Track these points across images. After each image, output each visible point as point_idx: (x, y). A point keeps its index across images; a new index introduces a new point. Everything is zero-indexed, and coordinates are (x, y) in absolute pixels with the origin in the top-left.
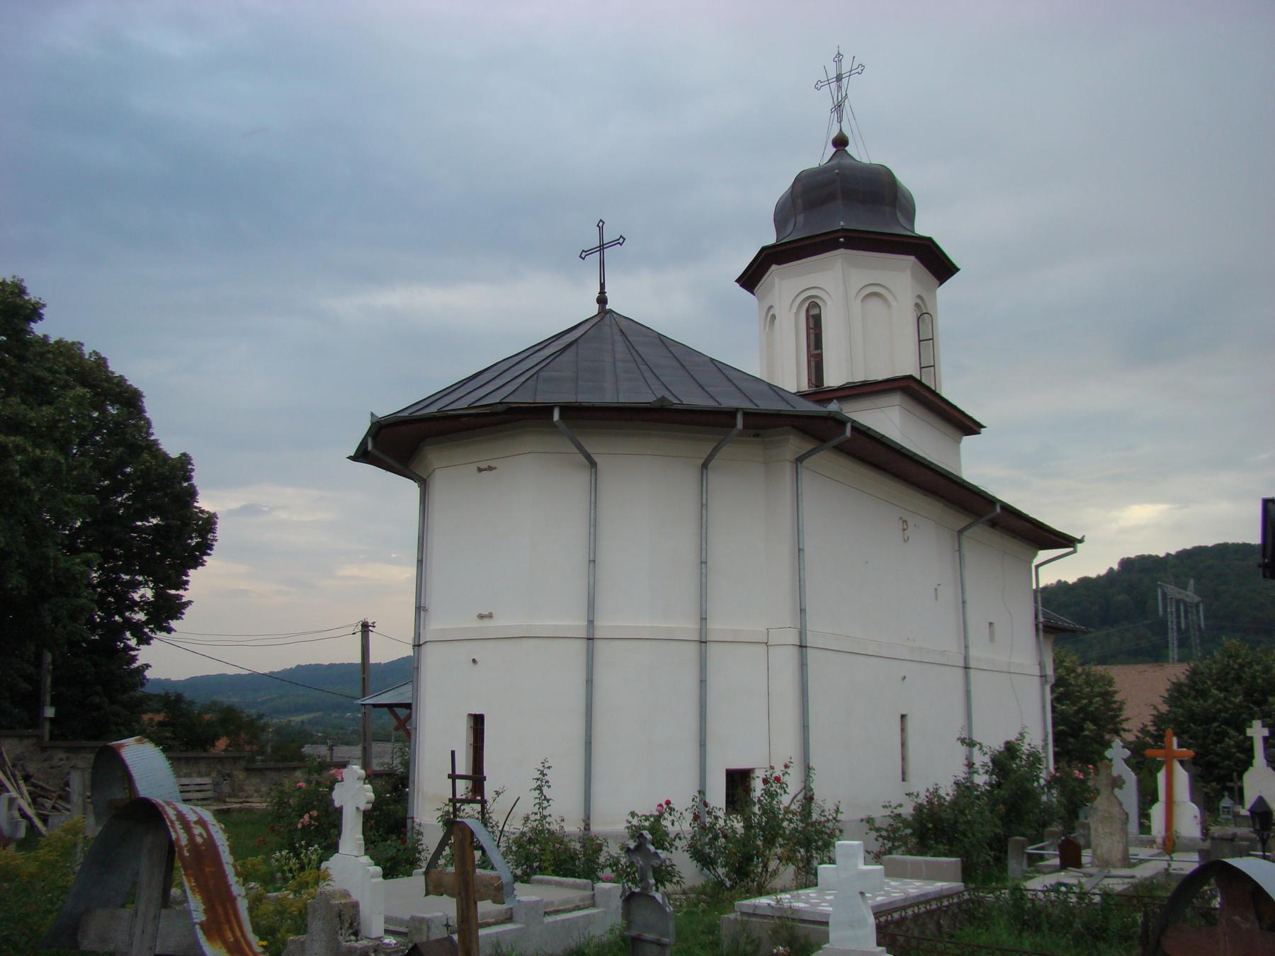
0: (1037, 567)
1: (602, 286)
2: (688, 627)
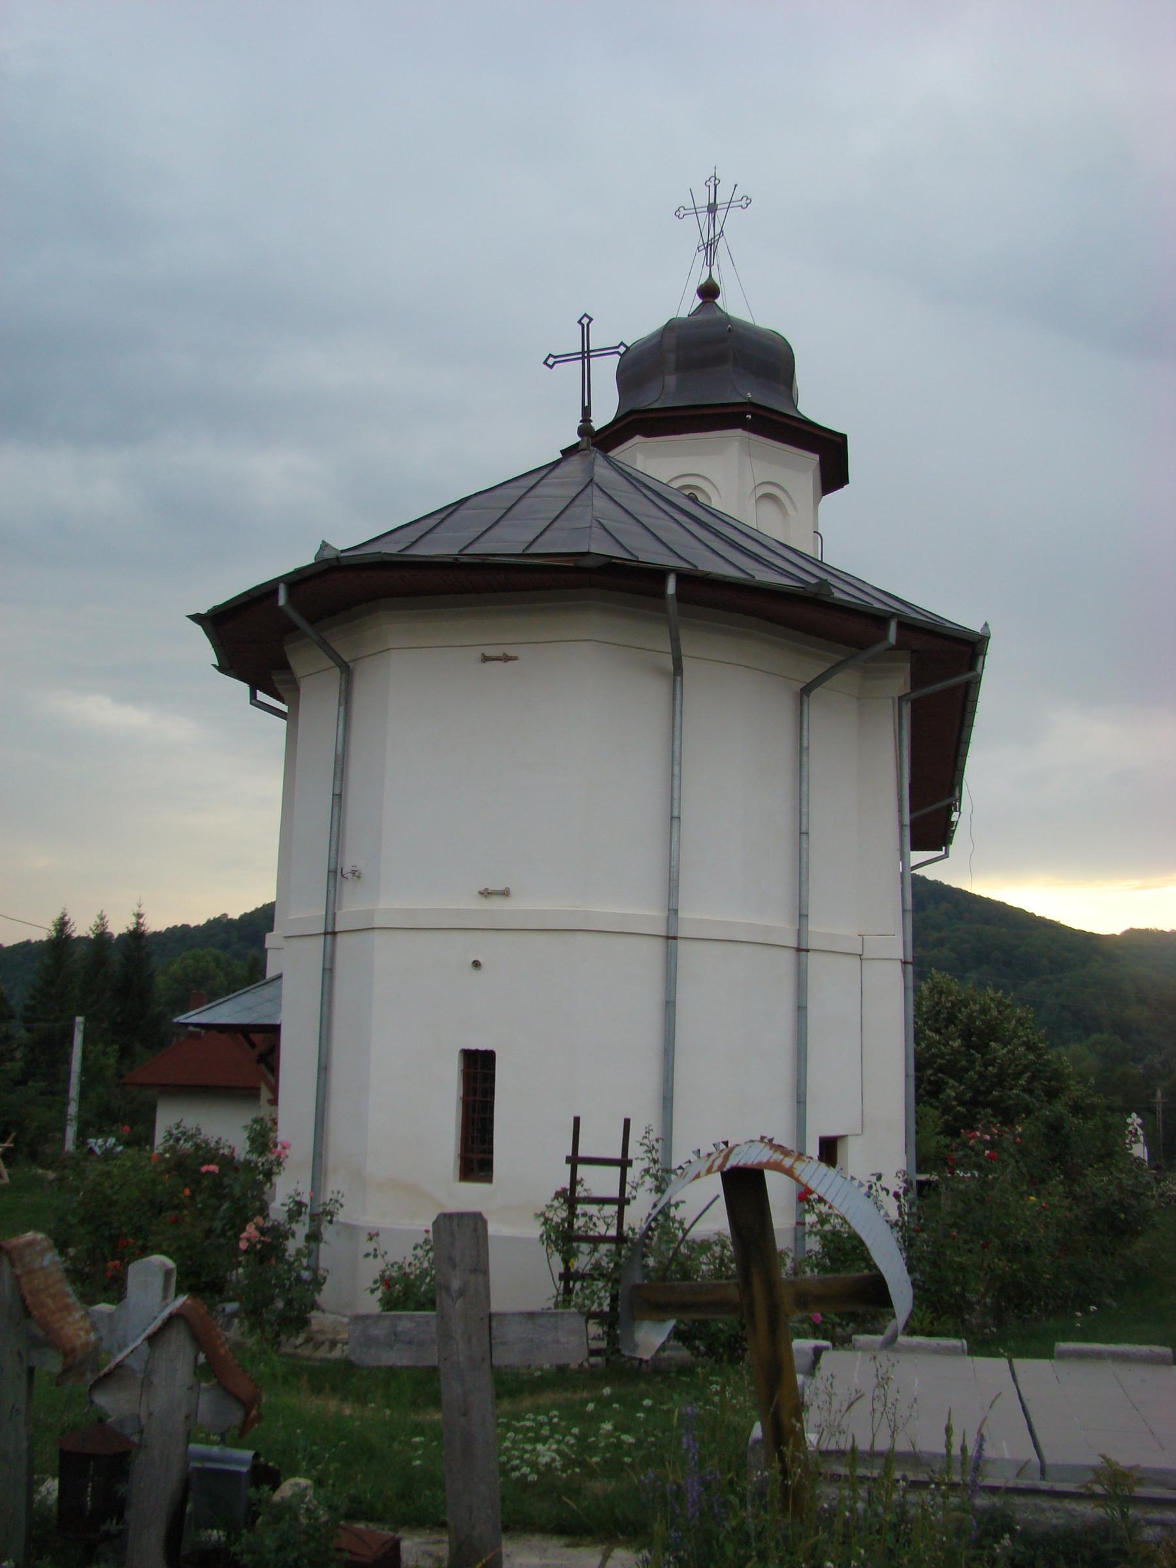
2: (782, 928)
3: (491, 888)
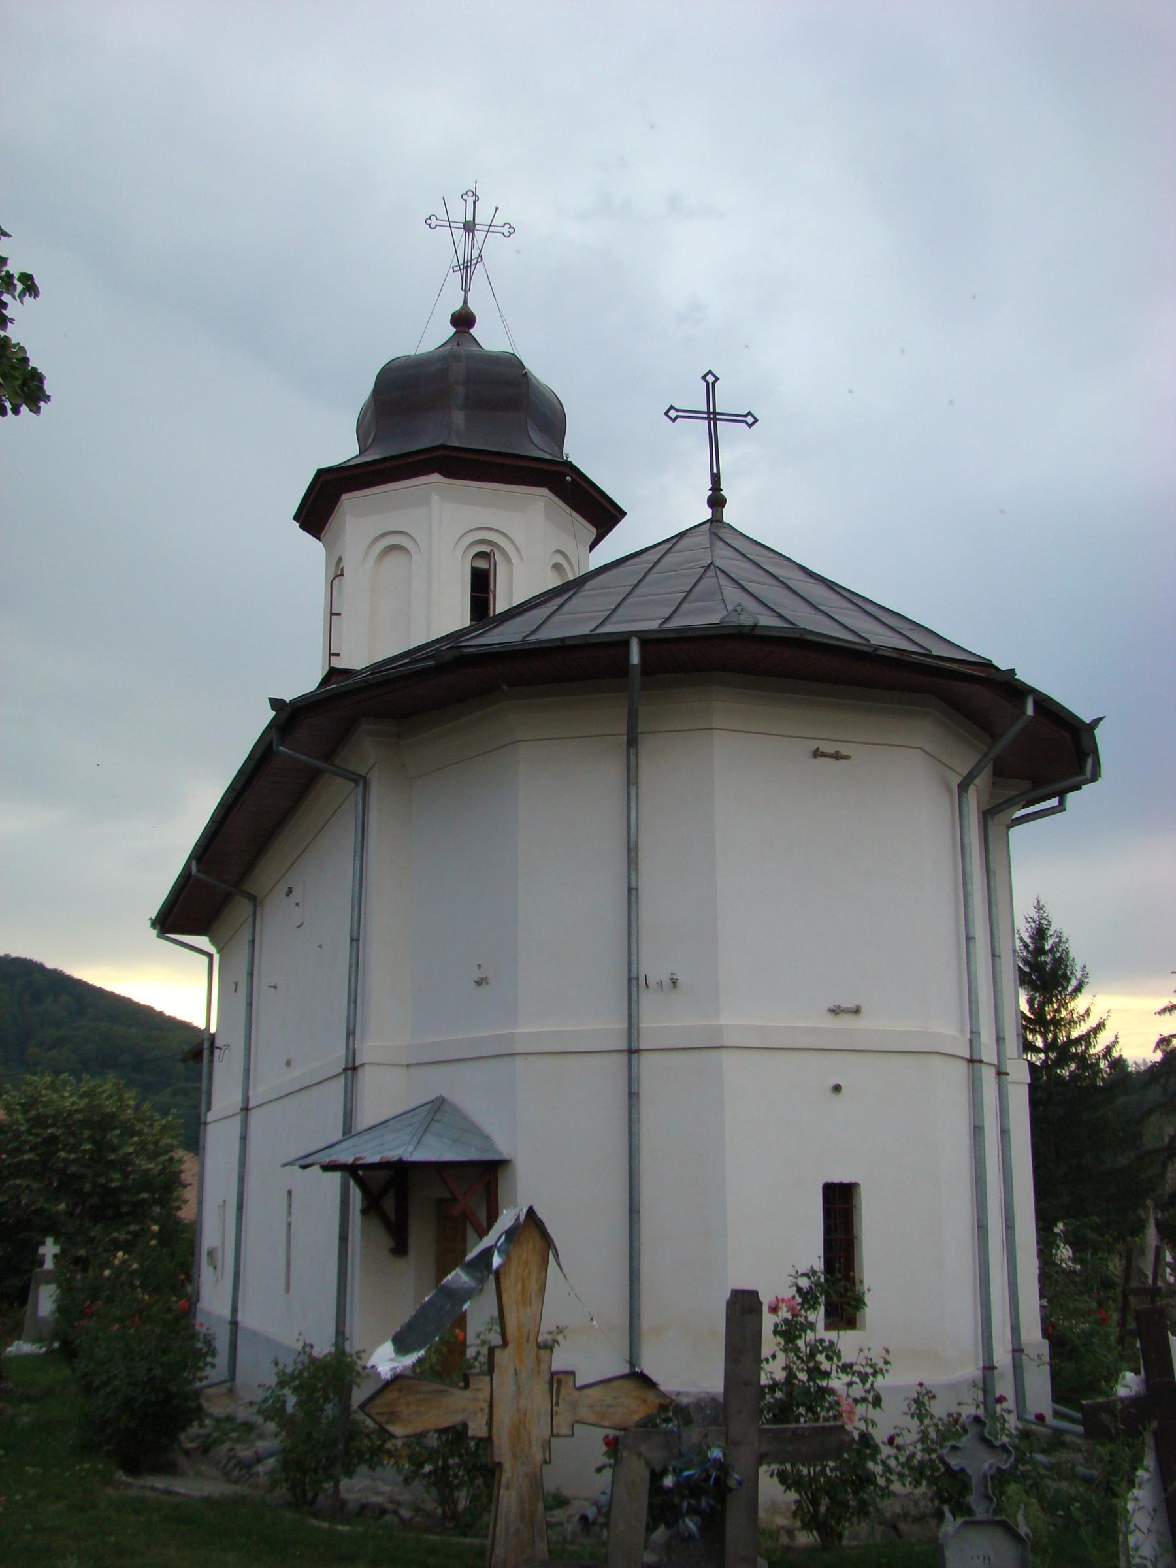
0: (210, 956)
1: (715, 478)
3: (844, 1005)
